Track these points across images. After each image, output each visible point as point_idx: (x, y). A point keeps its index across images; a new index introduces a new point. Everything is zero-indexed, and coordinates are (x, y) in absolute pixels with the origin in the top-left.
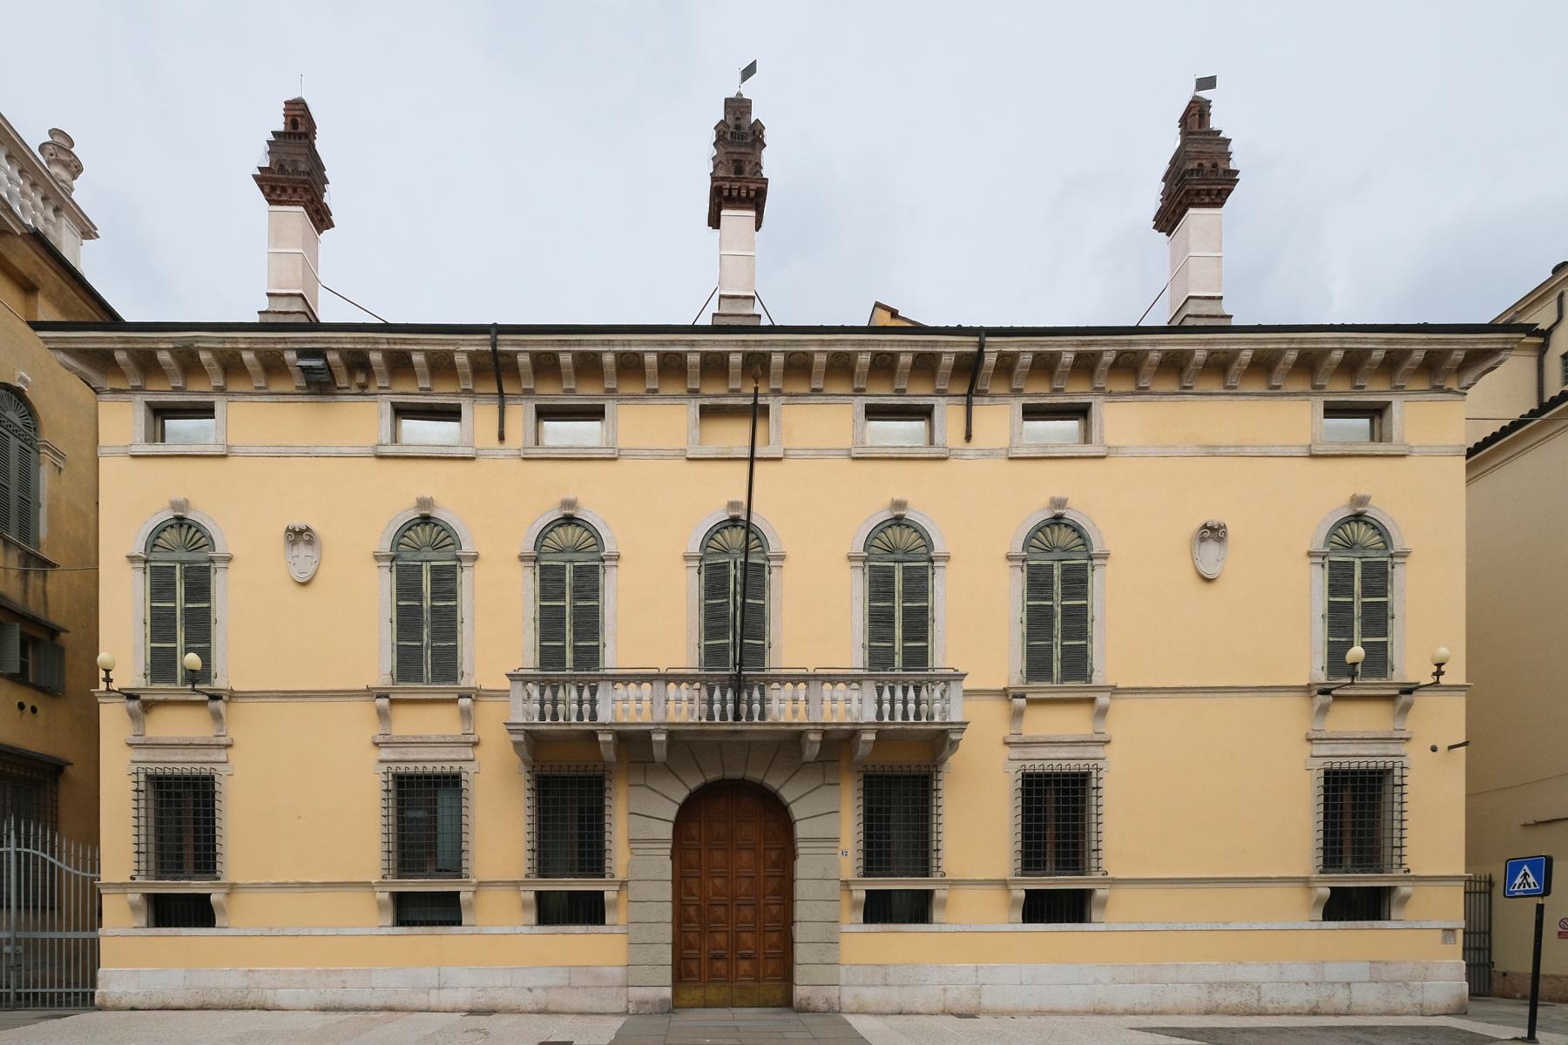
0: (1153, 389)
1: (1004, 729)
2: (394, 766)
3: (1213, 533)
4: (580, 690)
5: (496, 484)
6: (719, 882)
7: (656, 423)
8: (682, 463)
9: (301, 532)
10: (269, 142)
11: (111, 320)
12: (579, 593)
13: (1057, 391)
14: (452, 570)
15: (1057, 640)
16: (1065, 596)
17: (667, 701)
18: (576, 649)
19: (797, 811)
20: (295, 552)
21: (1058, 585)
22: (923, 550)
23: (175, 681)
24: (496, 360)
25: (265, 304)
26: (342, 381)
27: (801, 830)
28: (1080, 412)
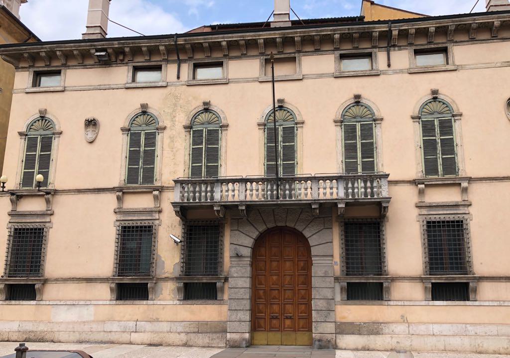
0: (477, 39)
2: (123, 222)
4: (365, 182)
5: (172, 97)
6: (275, 278)
7: (246, 68)
8: (407, 76)
9: (91, 121)
11: (38, 42)
12: (209, 141)
13: (430, 43)
14: (154, 134)
15: (440, 155)
16: (442, 134)
17: (246, 190)
18: (207, 167)
19: (312, 242)
20: (88, 130)
22: (370, 116)
23: (32, 186)
24: (176, 47)
25: (85, 31)
26: (113, 59)
27: (314, 251)
28: (444, 50)
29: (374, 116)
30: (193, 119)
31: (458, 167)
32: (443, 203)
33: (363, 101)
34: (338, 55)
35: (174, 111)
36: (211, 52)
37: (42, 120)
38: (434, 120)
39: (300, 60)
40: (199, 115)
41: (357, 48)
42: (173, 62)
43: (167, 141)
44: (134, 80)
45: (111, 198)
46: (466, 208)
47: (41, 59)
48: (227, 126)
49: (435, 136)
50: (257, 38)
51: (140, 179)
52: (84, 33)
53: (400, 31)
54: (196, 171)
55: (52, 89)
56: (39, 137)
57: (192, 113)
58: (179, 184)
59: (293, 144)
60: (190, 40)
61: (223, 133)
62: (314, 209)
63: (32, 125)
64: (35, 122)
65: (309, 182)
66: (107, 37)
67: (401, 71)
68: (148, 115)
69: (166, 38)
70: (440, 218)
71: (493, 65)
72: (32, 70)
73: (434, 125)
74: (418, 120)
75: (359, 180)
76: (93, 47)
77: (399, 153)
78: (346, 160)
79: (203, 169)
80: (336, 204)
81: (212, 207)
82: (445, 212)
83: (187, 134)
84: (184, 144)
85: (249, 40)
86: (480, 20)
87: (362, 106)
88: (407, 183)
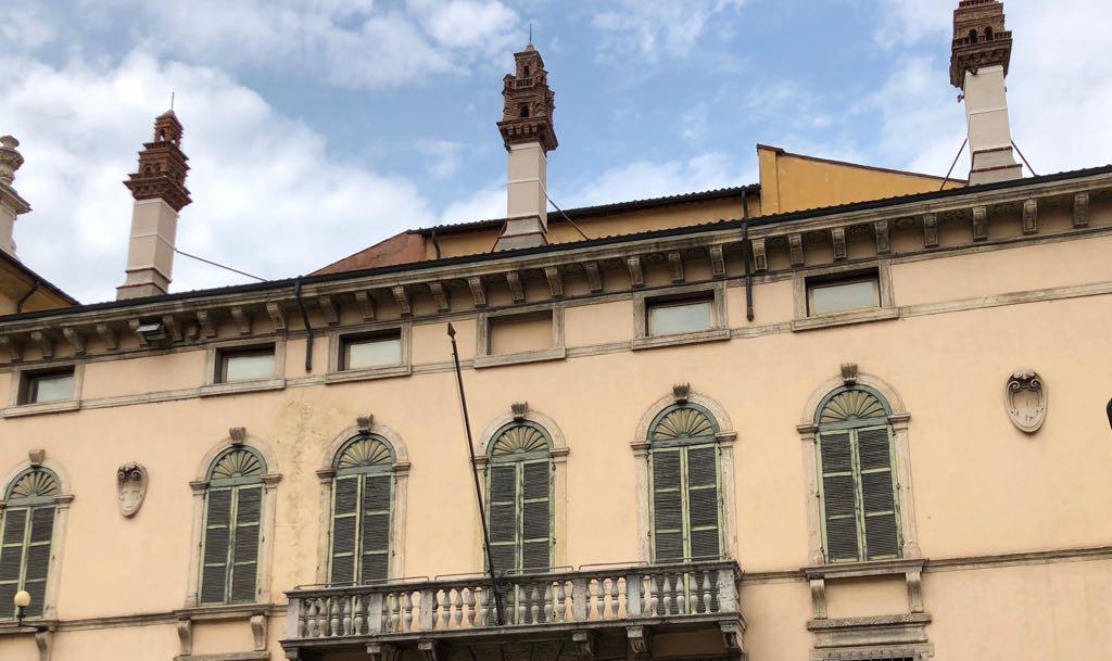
0: (942, 246)
1: (806, 612)
3: (1025, 386)
5: (294, 410)
7: (604, 322)
9: (131, 470)
10: (141, 154)
11: (76, 307)
12: (368, 503)
13: (839, 261)
14: (256, 493)
15: (861, 513)
16: (865, 464)
20: (125, 490)
21: (857, 457)
25: (123, 280)
26: (177, 336)
28: (872, 275)
29: (718, 431)
30: (338, 456)
31: (901, 536)
32: (866, 619)
33: (695, 399)
34: (642, 301)
35: (299, 440)
36: (804, 254)
37: (36, 473)
38: (886, 430)
39: (560, 317)
40: (349, 447)
41: (681, 283)
42: (298, 335)
43: (283, 506)
44: (219, 377)
45: (167, 634)
46: (919, 630)
47: (35, 345)
48: (408, 467)
49: (850, 469)
50: (466, 275)
51: (228, 590)
52: (121, 285)
53: (769, 241)
54: (340, 568)
55: (55, 407)
56: (29, 509)
57: (335, 444)
58: (298, 600)
59: (546, 499)
60: (330, 288)
61: (400, 482)
62: (579, 642)
63: (16, 485)
64: (22, 479)
65: (416, 594)
66: (172, 289)
67: (778, 328)
68: (247, 452)
69: (278, 287)
70: (861, 654)
71: (979, 303)
72: (16, 369)
73: (846, 444)
74: (812, 435)
75: (686, 575)
76: (134, 316)
77: (772, 510)
78: (659, 532)
79: (356, 564)
80: (624, 630)
81: (363, 647)
82: (873, 640)
83: (326, 489)
84: (318, 512)
85: (450, 280)
86: (938, 207)
87: (692, 410)
88: (789, 577)
